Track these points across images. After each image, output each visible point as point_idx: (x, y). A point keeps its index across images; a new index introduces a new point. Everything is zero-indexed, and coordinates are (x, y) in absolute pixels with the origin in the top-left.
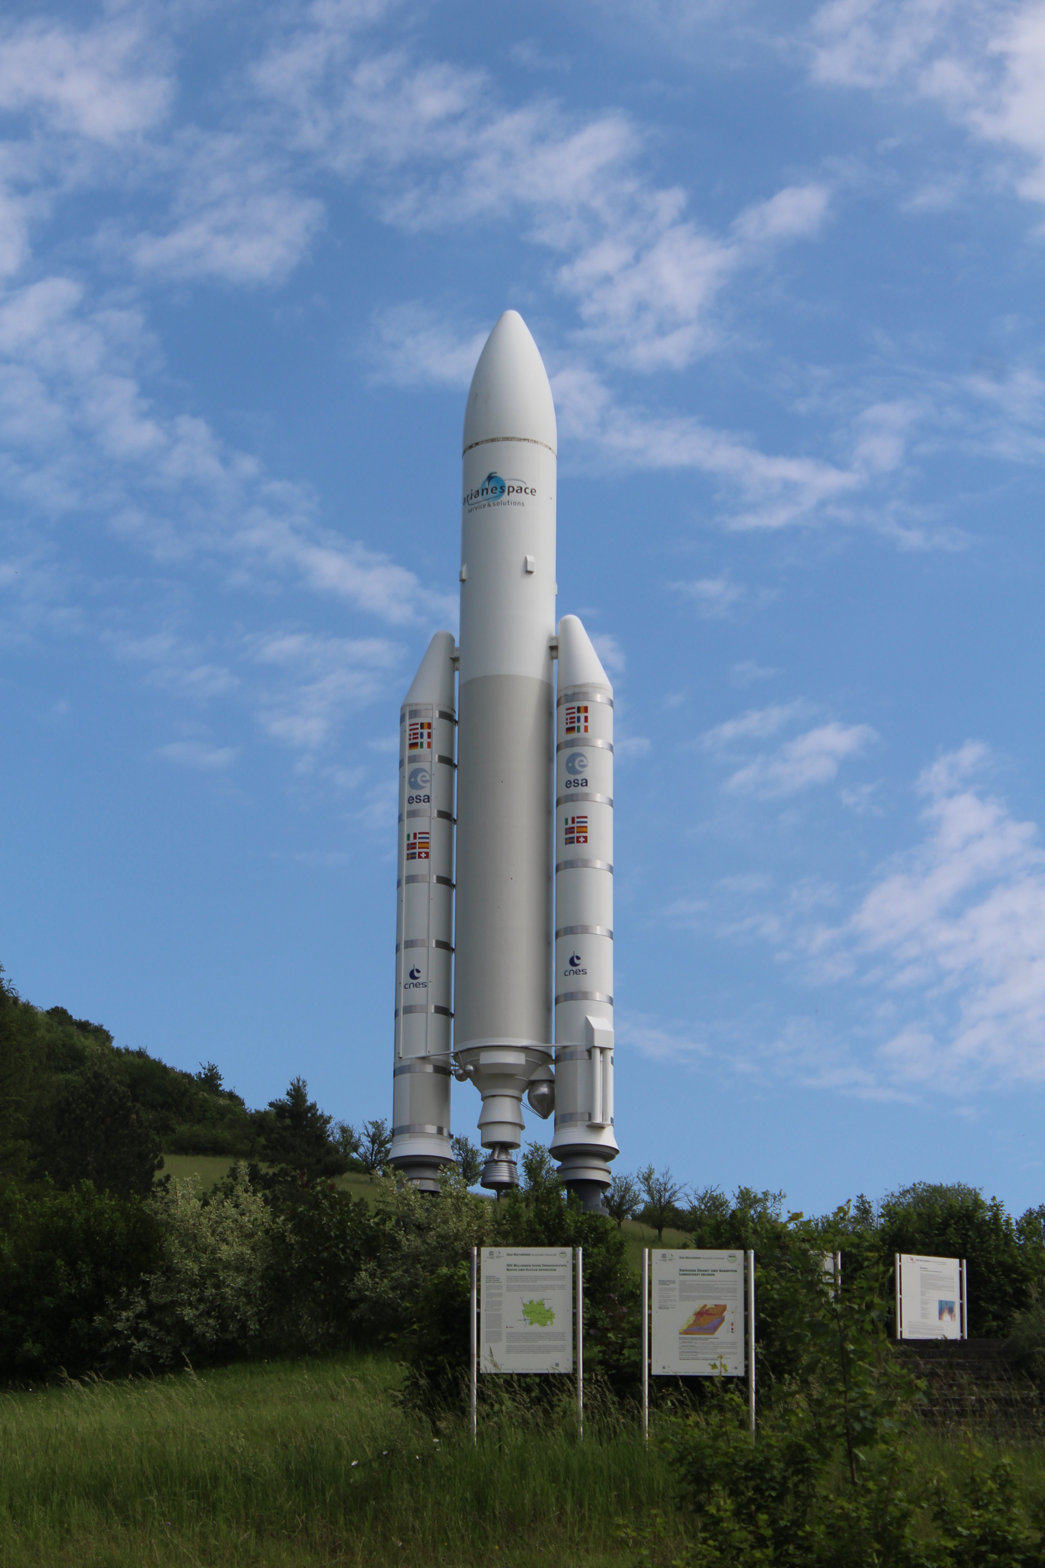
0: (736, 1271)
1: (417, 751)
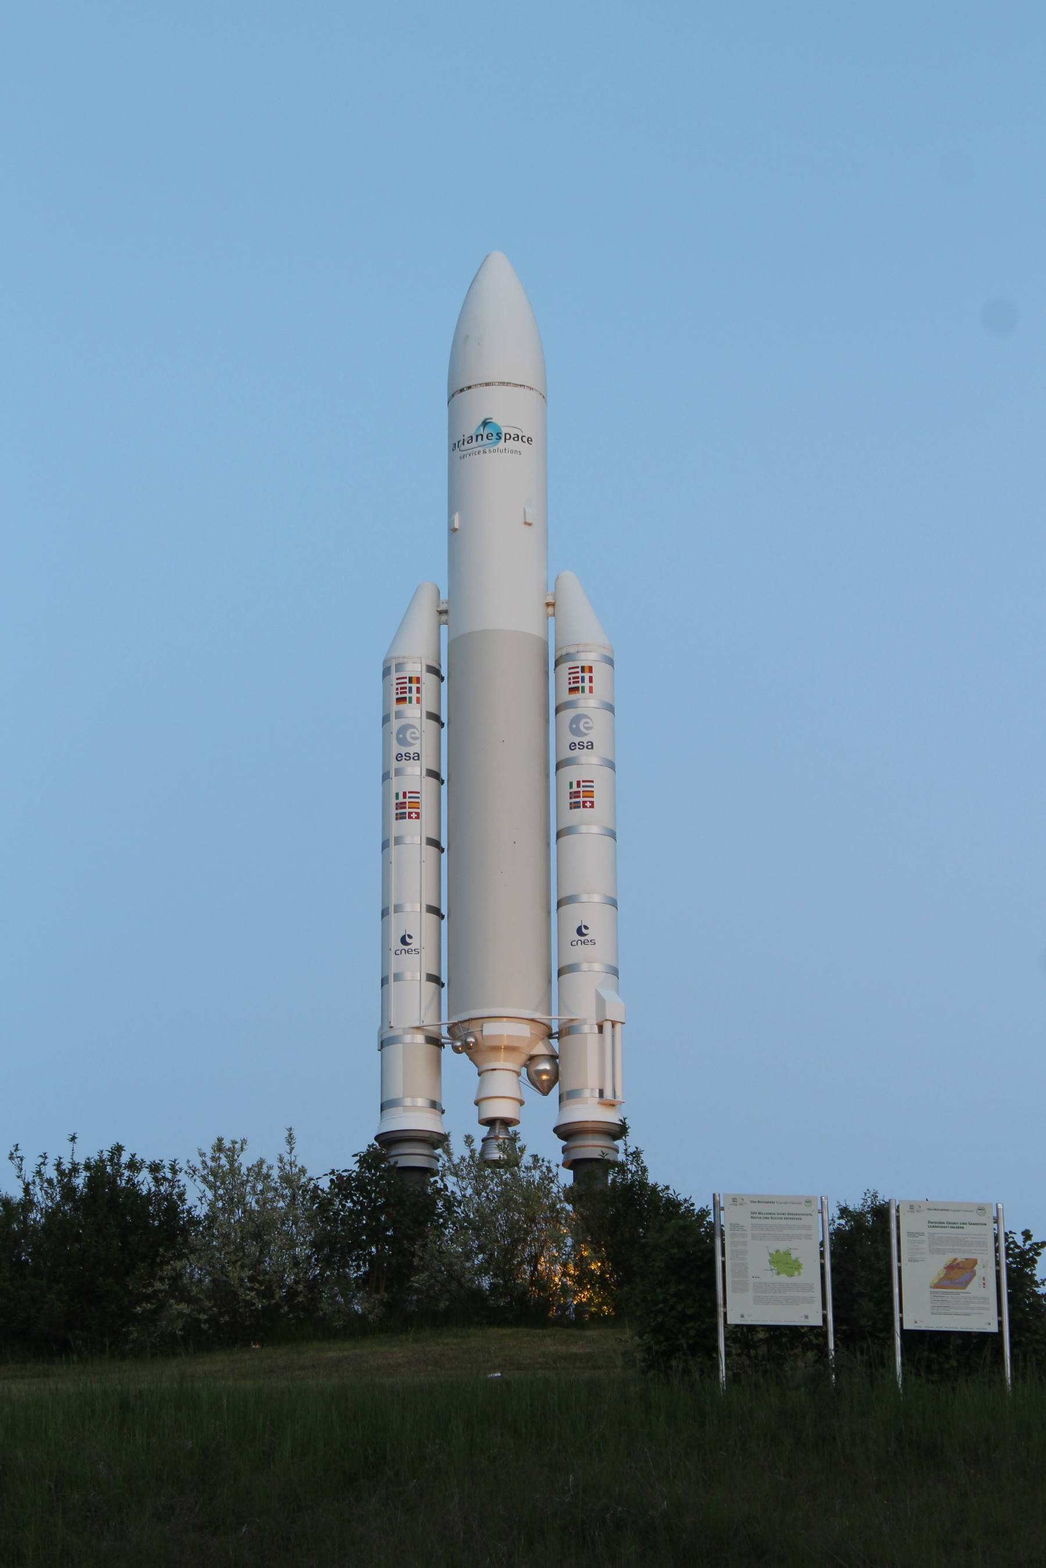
0: (985, 1224)
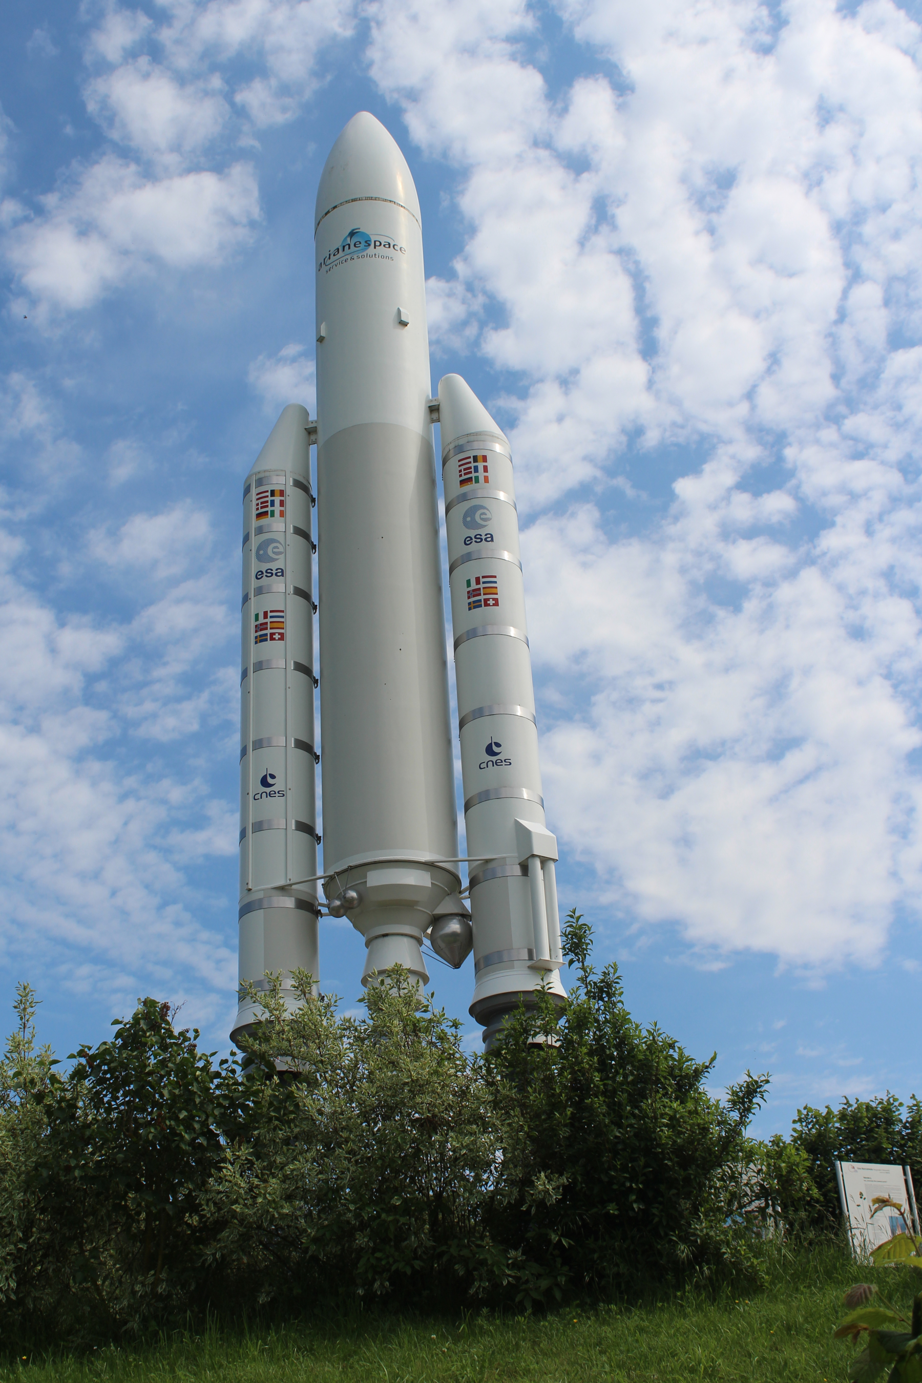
1: (264, 521)
